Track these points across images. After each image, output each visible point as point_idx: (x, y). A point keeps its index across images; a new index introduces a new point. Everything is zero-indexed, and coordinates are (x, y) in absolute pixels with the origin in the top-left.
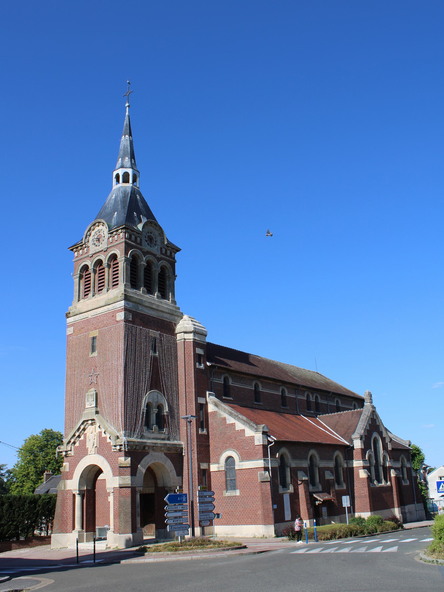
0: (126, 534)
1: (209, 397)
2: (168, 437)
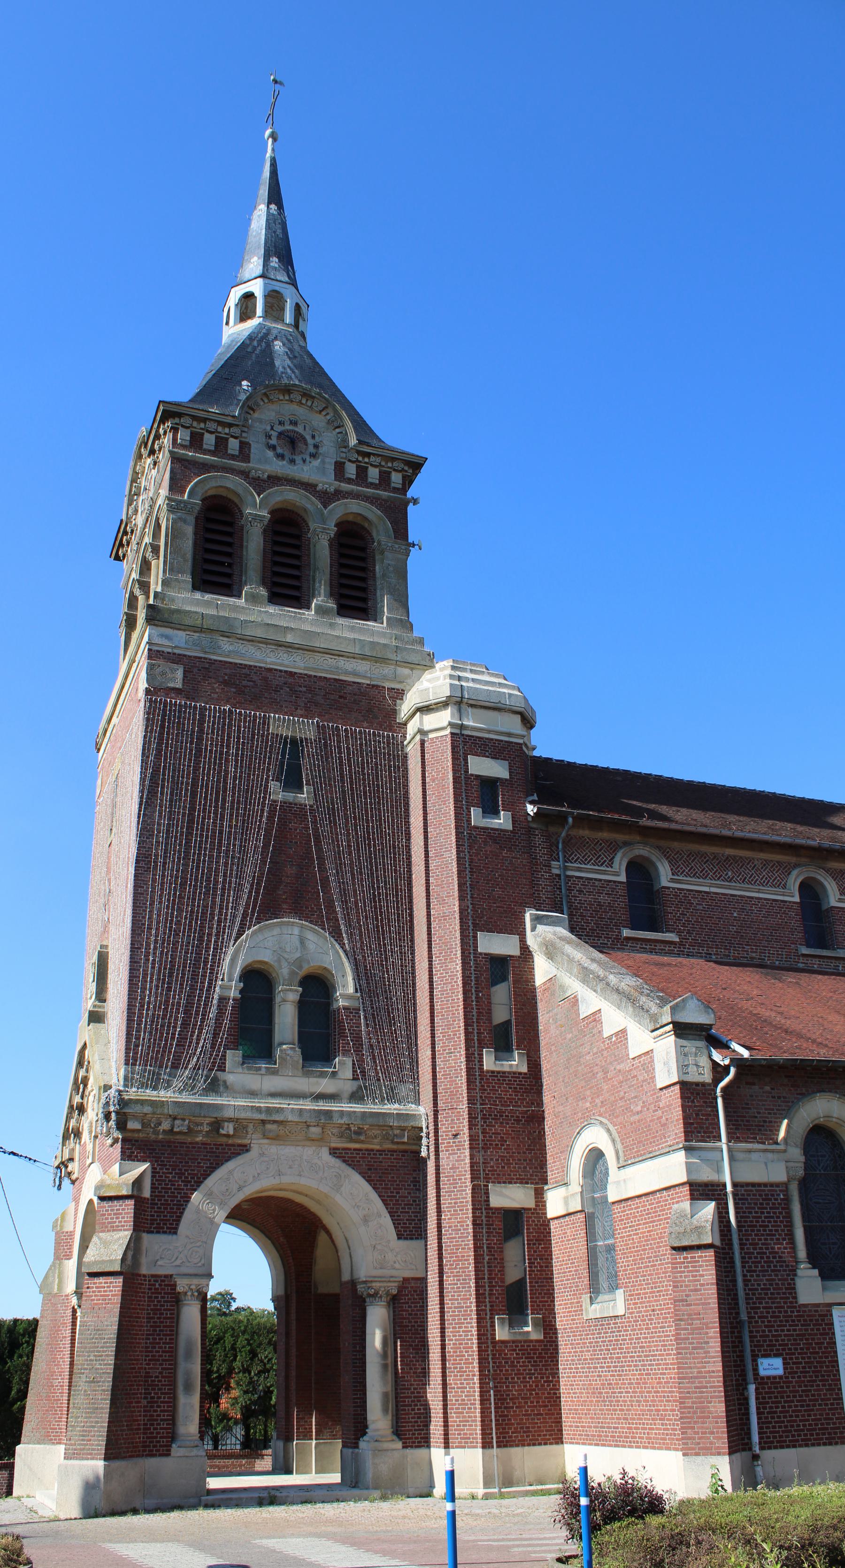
0: (87, 1459)
1: (533, 929)
2: (355, 1089)
